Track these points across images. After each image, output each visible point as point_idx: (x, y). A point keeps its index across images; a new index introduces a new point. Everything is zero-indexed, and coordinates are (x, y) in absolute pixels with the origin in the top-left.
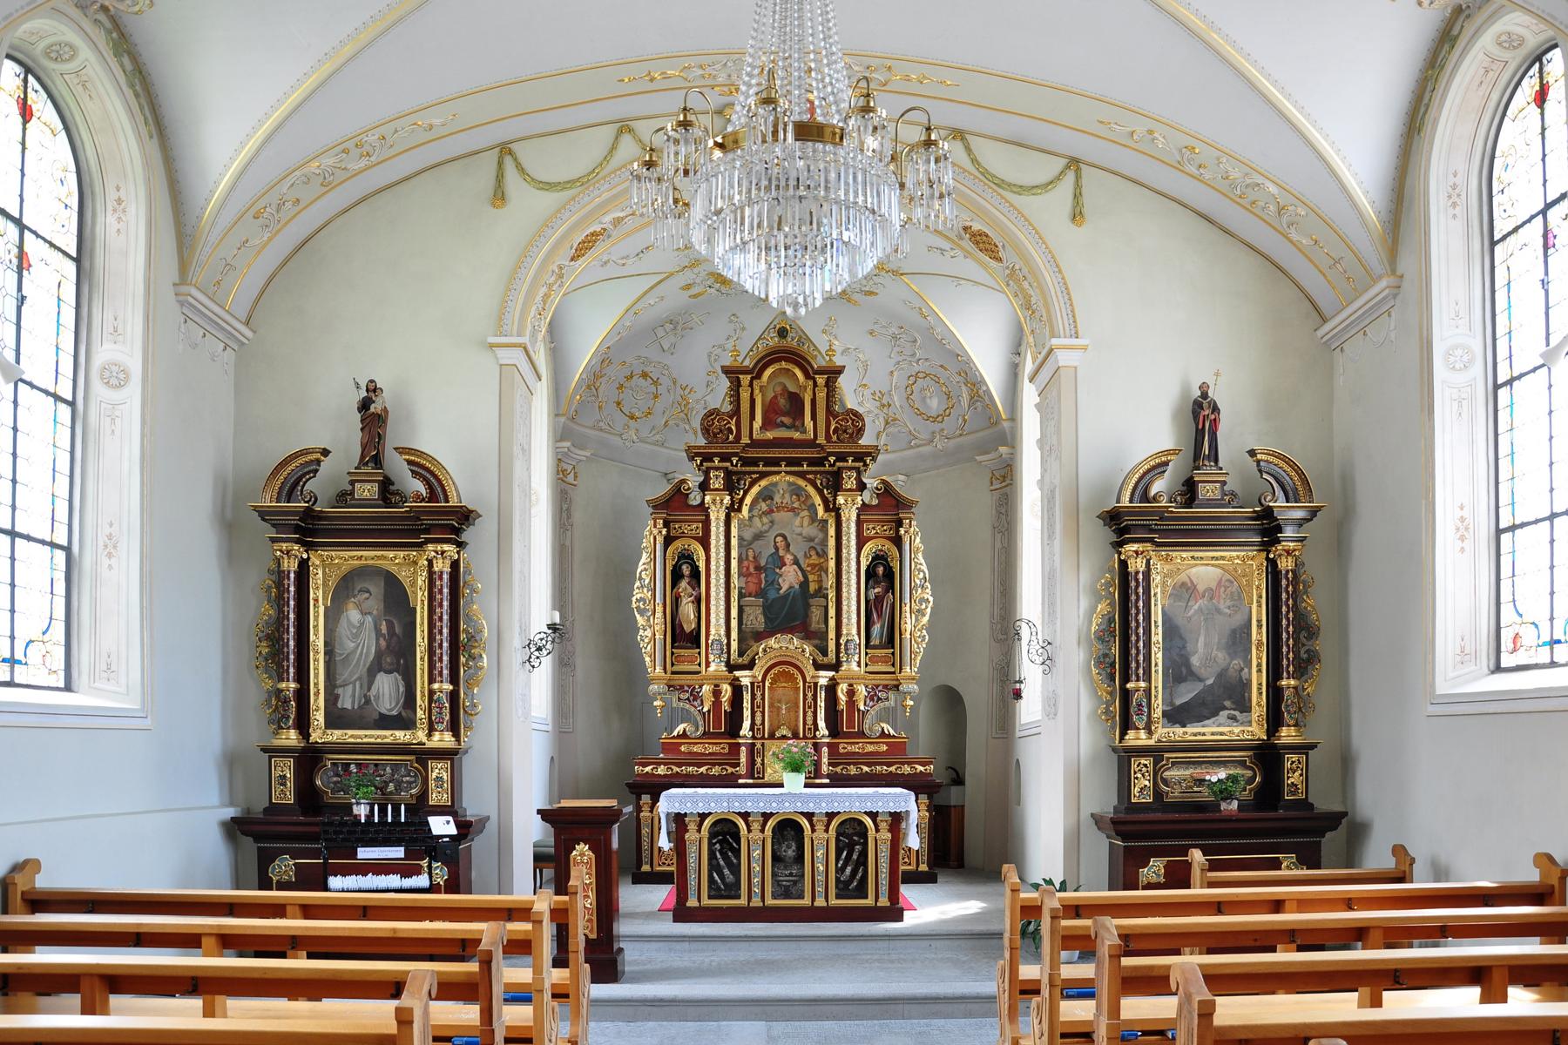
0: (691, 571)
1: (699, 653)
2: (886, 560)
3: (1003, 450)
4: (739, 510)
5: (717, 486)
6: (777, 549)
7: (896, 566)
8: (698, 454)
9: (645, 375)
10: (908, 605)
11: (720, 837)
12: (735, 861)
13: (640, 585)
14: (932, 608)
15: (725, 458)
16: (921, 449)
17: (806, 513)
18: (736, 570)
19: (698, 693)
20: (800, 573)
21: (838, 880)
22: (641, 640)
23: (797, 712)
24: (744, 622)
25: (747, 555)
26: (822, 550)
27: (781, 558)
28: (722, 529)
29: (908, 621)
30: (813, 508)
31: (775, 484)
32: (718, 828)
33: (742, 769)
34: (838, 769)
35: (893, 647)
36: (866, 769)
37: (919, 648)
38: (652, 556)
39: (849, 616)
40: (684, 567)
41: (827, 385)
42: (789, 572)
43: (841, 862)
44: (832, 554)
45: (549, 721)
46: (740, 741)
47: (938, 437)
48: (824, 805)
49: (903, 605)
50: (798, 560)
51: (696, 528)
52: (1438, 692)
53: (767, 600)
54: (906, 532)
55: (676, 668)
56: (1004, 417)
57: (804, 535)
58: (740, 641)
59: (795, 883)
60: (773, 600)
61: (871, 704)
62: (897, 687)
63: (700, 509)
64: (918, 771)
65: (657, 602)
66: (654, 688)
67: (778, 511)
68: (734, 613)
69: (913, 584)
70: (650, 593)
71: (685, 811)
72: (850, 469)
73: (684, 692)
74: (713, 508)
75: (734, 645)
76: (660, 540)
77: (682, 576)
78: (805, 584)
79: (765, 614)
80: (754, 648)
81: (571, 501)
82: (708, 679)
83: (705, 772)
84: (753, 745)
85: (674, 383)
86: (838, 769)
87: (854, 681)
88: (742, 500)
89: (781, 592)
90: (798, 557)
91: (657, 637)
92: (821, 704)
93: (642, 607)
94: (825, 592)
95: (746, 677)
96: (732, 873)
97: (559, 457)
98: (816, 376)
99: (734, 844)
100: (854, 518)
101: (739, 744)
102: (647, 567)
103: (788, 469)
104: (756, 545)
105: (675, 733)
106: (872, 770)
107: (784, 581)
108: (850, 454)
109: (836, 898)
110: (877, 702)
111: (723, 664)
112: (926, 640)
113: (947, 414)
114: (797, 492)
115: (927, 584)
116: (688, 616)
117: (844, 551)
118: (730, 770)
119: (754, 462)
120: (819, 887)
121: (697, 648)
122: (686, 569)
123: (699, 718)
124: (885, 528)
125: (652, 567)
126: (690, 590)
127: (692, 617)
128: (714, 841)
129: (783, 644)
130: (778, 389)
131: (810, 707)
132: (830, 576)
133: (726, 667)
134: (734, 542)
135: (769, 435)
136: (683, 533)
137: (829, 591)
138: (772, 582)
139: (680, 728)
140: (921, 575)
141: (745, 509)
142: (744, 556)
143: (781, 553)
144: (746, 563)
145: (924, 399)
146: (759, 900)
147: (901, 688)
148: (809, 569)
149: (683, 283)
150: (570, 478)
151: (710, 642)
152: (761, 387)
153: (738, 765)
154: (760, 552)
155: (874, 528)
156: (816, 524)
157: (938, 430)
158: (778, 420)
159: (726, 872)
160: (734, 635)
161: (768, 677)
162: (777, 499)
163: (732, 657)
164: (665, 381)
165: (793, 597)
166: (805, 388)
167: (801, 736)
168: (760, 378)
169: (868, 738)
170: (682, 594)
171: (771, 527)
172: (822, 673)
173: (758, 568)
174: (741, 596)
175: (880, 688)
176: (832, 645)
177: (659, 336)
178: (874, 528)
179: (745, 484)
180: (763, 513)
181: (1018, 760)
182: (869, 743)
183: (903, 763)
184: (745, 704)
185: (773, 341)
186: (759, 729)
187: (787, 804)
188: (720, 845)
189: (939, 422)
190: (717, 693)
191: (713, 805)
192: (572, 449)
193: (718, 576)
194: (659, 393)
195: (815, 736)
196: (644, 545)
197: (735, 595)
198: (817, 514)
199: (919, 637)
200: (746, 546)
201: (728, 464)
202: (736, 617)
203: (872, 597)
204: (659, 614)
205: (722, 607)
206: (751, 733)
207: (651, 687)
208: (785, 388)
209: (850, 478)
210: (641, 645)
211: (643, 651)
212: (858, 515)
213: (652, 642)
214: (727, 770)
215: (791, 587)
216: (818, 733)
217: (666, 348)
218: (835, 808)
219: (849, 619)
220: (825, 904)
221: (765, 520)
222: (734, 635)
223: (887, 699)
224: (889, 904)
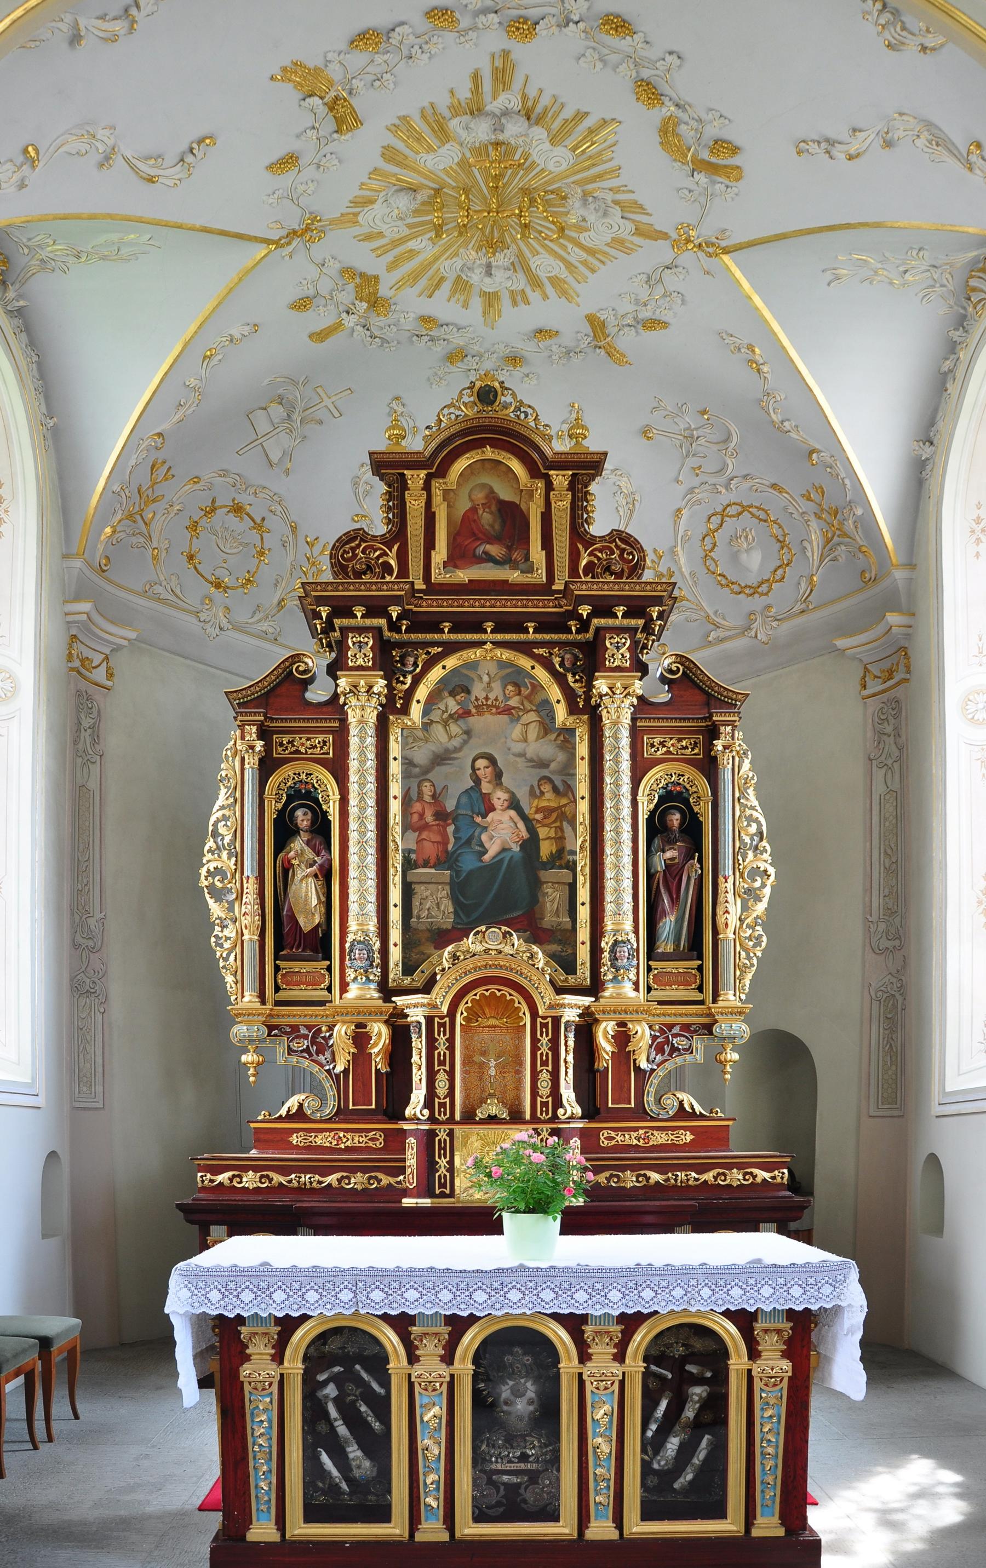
0: (313, 822)
1: (329, 969)
2: (686, 802)
3: (893, 618)
4: (405, 711)
5: (360, 662)
6: (477, 781)
7: (704, 810)
8: (320, 601)
9: (238, 509)
10: (731, 880)
11: (337, 1369)
12: (377, 1426)
13: (214, 846)
14: (772, 887)
15: (376, 608)
16: (728, 645)
17: (532, 716)
18: (399, 819)
19: (326, 1039)
20: (521, 825)
21: (646, 1468)
22: (217, 944)
23: (519, 1072)
24: (415, 912)
25: (420, 793)
26: (564, 782)
27: (486, 799)
28: (371, 741)
29: (731, 908)
30: (545, 708)
31: (473, 665)
32: (333, 1346)
33: (410, 1179)
34: (602, 1178)
35: (700, 957)
36: (655, 1177)
37: (749, 958)
38: (238, 795)
39: (618, 898)
40: (299, 813)
41: (572, 487)
42: (500, 822)
43: (654, 1427)
44: (583, 789)
45: (41, 1087)
46: (406, 1127)
47: (759, 620)
48: (615, 1295)
49: (721, 879)
50: (518, 801)
51: (322, 743)
52: (948, 1089)
53: (458, 873)
54: (725, 747)
55: (282, 995)
56: (894, 561)
57: (528, 756)
58: (408, 945)
59: (533, 1477)
60: (471, 872)
61: (659, 1058)
62: (708, 1029)
63: (330, 708)
64: (759, 1180)
65: (246, 874)
66: (240, 1031)
67: (480, 713)
68: (395, 895)
69: (737, 845)
70: (234, 859)
71: (237, 1311)
72: (619, 630)
73: (297, 1037)
74: (353, 701)
75: (395, 954)
76: (252, 762)
77: (296, 832)
78: (531, 844)
79: (454, 898)
80: (434, 959)
81: (99, 712)
82: (344, 1012)
83: (335, 1184)
84: (431, 1134)
85: (294, 529)
86: (602, 1178)
87: (628, 1017)
88: (409, 695)
89: (487, 857)
90: (519, 796)
91: (246, 937)
92: (568, 1057)
93: (219, 885)
94: (571, 858)
95: (416, 1006)
96: (368, 1452)
97: (74, 632)
98: (551, 472)
99: (375, 1386)
100: (626, 720)
101: (404, 1131)
102: (226, 812)
103: (499, 637)
104: (437, 775)
105: (283, 1112)
106: (667, 1180)
107: (491, 838)
108: (621, 600)
109: (643, 1519)
110: (670, 1055)
111: (373, 986)
112: (764, 945)
113: (778, 577)
114: (516, 678)
115: (764, 843)
116: (307, 900)
117: (608, 779)
118: (386, 1180)
119: (431, 624)
120: (598, 1493)
121: (324, 959)
122: (302, 818)
123: (328, 1084)
124: (684, 743)
125: (238, 814)
126: (310, 854)
127: (314, 902)
128: (322, 1377)
129: (492, 945)
130: (480, 496)
131: (544, 1063)
132: (580, 829)
133: (380, 991)
134: (395, 768)
135: (463, 576)
136: (297, 752)
137: (578, 857)
138: (469, 842)
139: (293, 1103)
140: (753, 829)
141: (416, 710)
142: (414, 794)
143: (486, 787)
144: (417, 807)
145: (735, 557)
146: (440, 1525)
147: (716, 1029)
148: (539, 817)
149: (293, 294)
150: (99, 675)
151: (347, 945)
152: (446, 493)
153: (402, 1170)
154: (445, 787)
155: (662, 744)
156: (553, 736)
157: (759, 609)
158: (480, 550)
159: (354, 1452)
160: (395, 935)
161: (462, 1007)
162: (478, 691)
163: (391, 976)
164: (273, 523)
165: (509, 865)
166: (531, 494)
167: (528, 1116)
168: (444, 477)
169: (653, 1119)
170: (295, 862)
171: (465, 742)
172: (569, 999)
173: (442, 815)
174: (408, 864)
175: (676, 1030)
176: (583, 954)
177: (261, 431)
178: (662, 744)
179: (415, 665)
180: (451, 716)
181: (933, 1161)
182: (658, 1129)
183: (730, 1167)
184: (415, 1058)
185: (469, 411)
186: (442, 1105)
187: (514, 1296)
188: (339, 1387)
189: (762, 594)
190: (361, 1039)
191: (312, 1296)
192: (97, 618)
193: (362, 824)
194: (266, 546)
195: (555, 1117)
196: (223, 773)
197: (396, 861)
198: (554, 718)
199: (750, 938)
200: (416, 776)
201: (382, 622)
202: (399, 903)
203: (659, 865)
204: (250, 895)
205: (371, 884)
206: (426, 1112)
207: (235, 1029)
208: (491, 495)
209: (618, 648)
210: (218, 954)
211: (221, 964)
212: (634, 720)
213: (238, 949)
214: (379, 1181)
215: (504, 850)
216: (561, 1111)
217: (275, 458)
218: (645, 1301)
219: (618, 904)
220: (613, 1535)
221: (454, 728)
222: (395, 935)
223: (689, 1050)
224: (781, 1532)
